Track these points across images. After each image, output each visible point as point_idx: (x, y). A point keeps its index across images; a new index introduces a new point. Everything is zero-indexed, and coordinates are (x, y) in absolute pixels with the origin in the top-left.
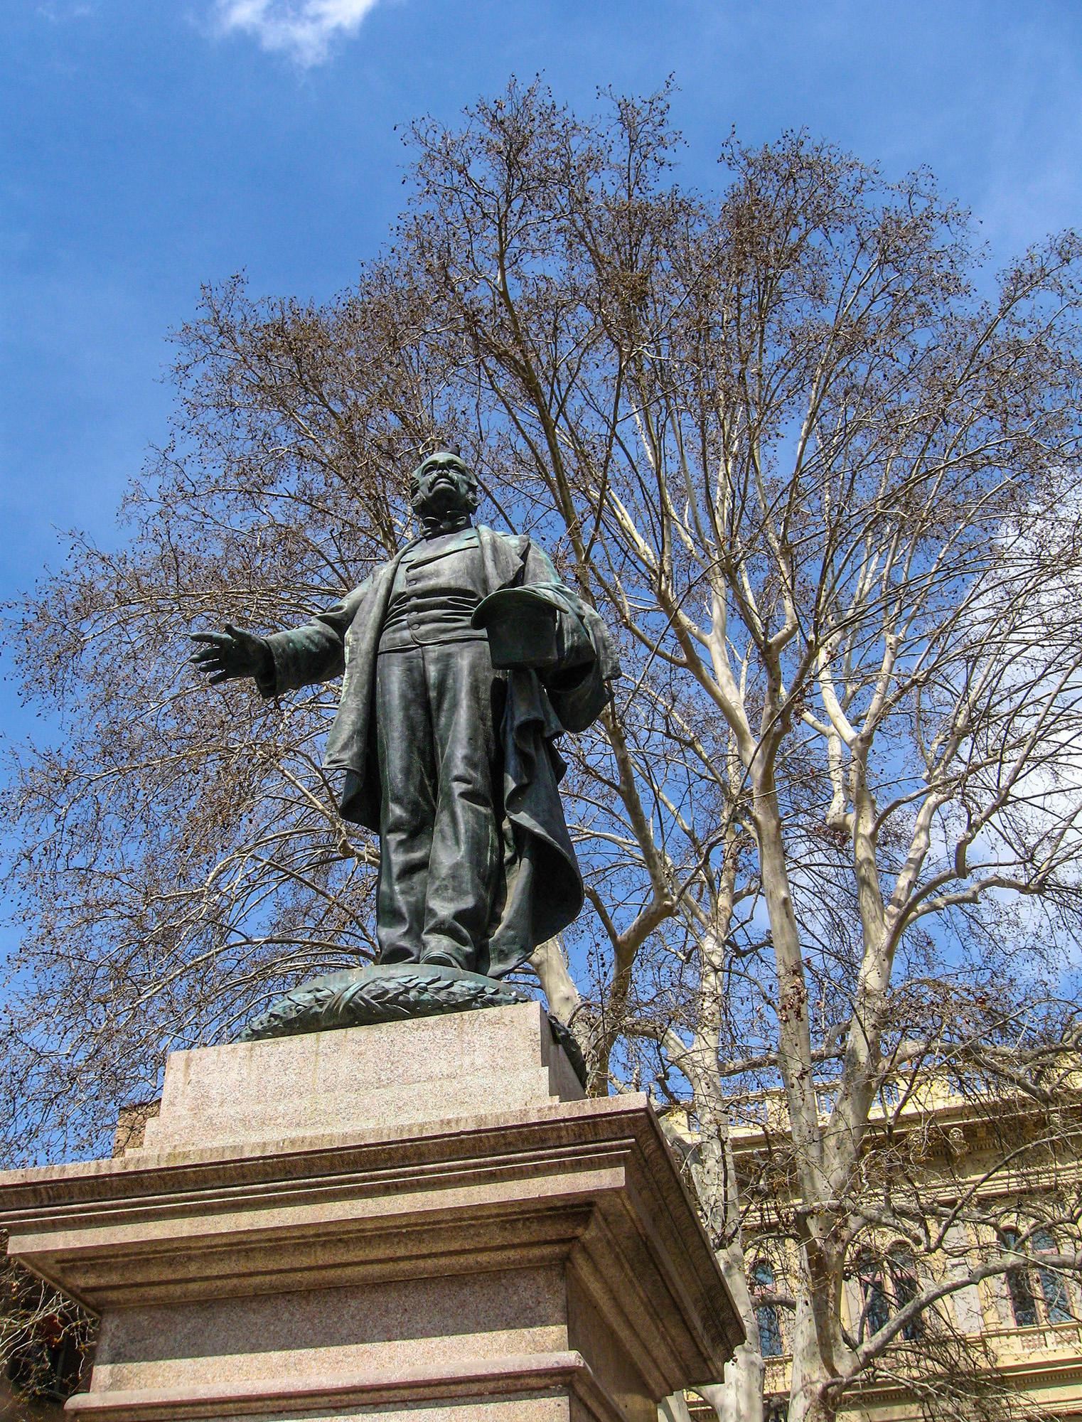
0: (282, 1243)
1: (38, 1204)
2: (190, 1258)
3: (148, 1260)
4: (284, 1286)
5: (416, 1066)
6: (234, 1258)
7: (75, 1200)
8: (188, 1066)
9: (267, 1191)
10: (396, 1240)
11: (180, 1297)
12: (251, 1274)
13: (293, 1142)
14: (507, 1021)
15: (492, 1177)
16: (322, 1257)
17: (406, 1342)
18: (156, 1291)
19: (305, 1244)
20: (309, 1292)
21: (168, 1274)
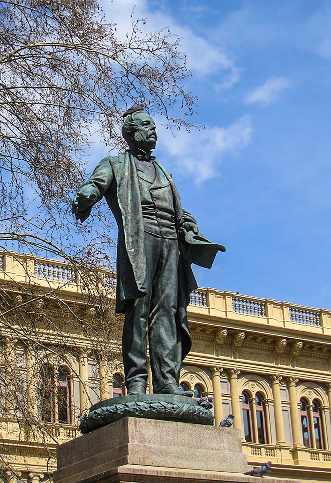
5: (208, 443)
8: (136, 424)
13: (214, 476)
14: (232, 433)
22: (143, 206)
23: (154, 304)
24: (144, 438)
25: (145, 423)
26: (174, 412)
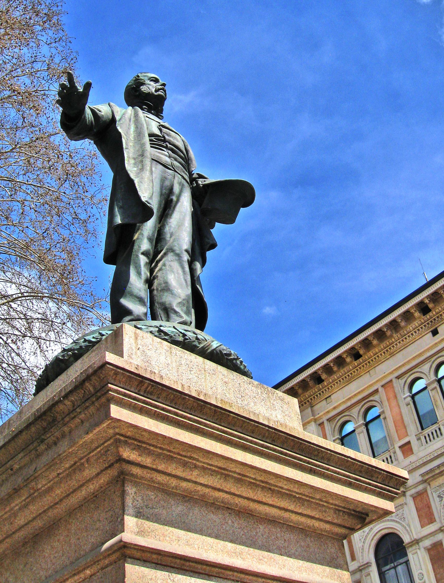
0: (244, 478)
1: (137, 391)
2: (196, 467)
3: (172, 457)
4: (228, 503)
6: (219, 477)
7: (160, 400)
9: (262, 446)
10: (293, 499)
11: (173, 488)
12: (219, 490)
15: (350, 485)
16: (260, 495)
17: (289, 559)
18: (161, 478)
19: (279, 492)
20: (239, 512)
21: (179, 472)
22: (150, 138)
23: (159, 250)
24: (150, 364)
25: (152, 342)
26: (198, 345)
